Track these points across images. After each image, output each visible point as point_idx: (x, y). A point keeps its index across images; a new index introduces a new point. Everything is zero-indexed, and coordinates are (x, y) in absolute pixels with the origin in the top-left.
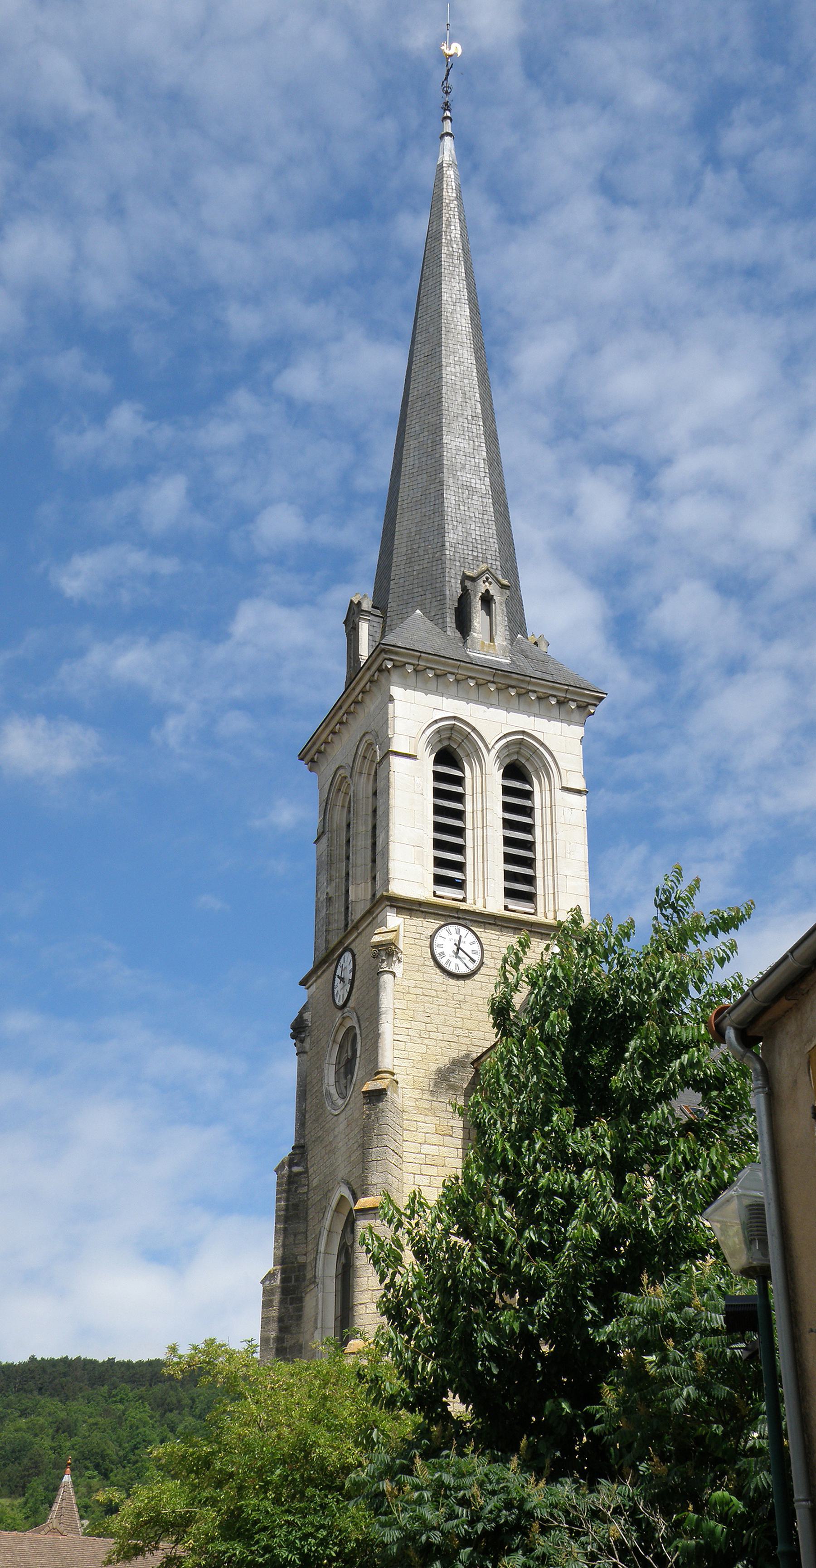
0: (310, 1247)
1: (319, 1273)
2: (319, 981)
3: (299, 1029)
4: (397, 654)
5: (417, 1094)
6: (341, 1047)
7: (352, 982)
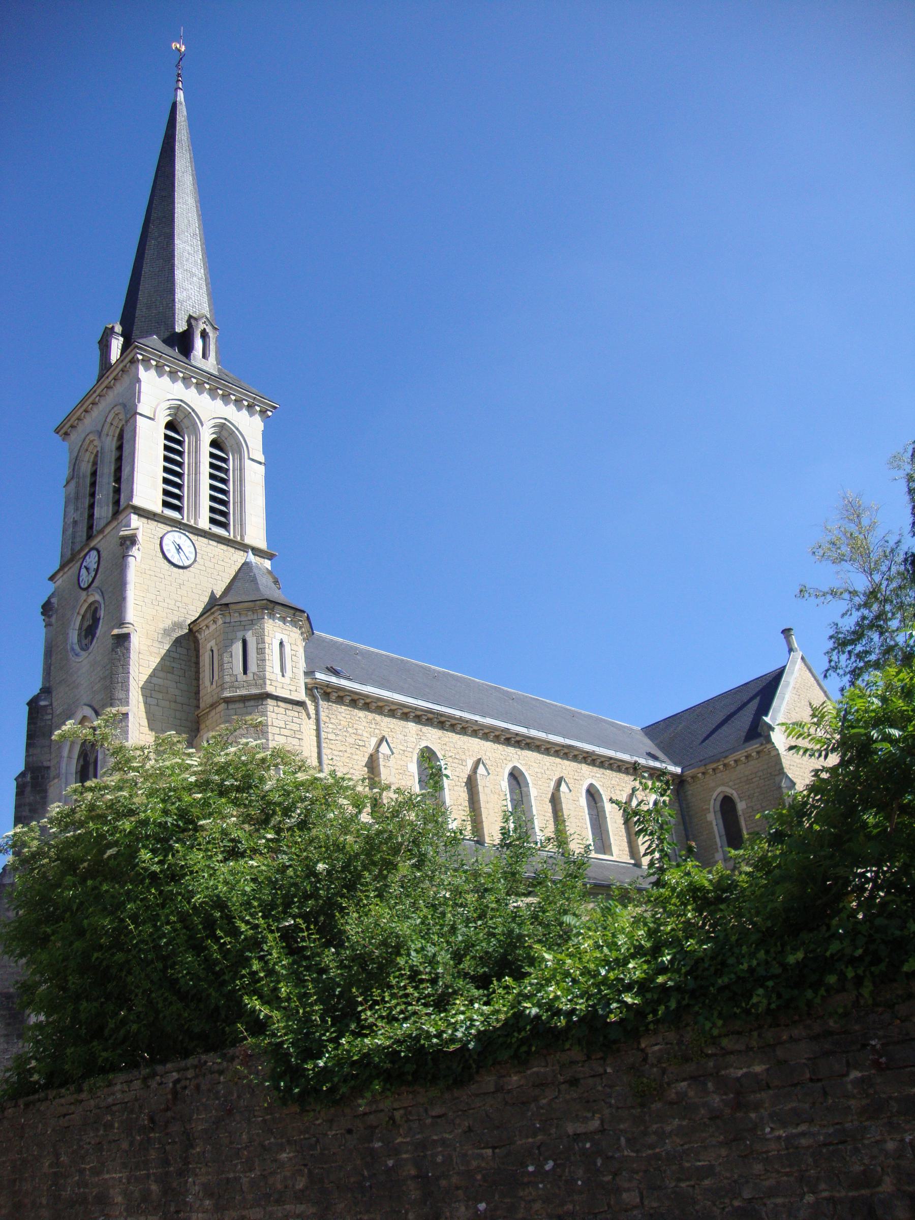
0: (53, 755)
1: (63, 771)
2: (65, 576)
3: (47, 609)
4: (145, 351)
5: (149, 642)
6: (83, 617)
7: (97, 571)
